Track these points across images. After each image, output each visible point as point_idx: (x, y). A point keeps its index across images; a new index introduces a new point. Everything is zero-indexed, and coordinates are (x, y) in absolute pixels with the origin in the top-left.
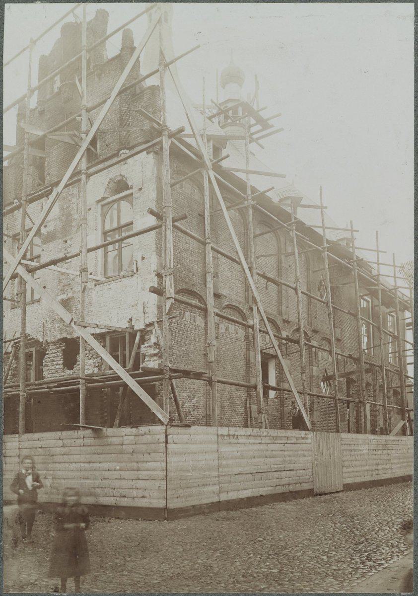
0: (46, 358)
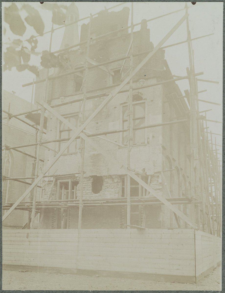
0: (79, 186)
